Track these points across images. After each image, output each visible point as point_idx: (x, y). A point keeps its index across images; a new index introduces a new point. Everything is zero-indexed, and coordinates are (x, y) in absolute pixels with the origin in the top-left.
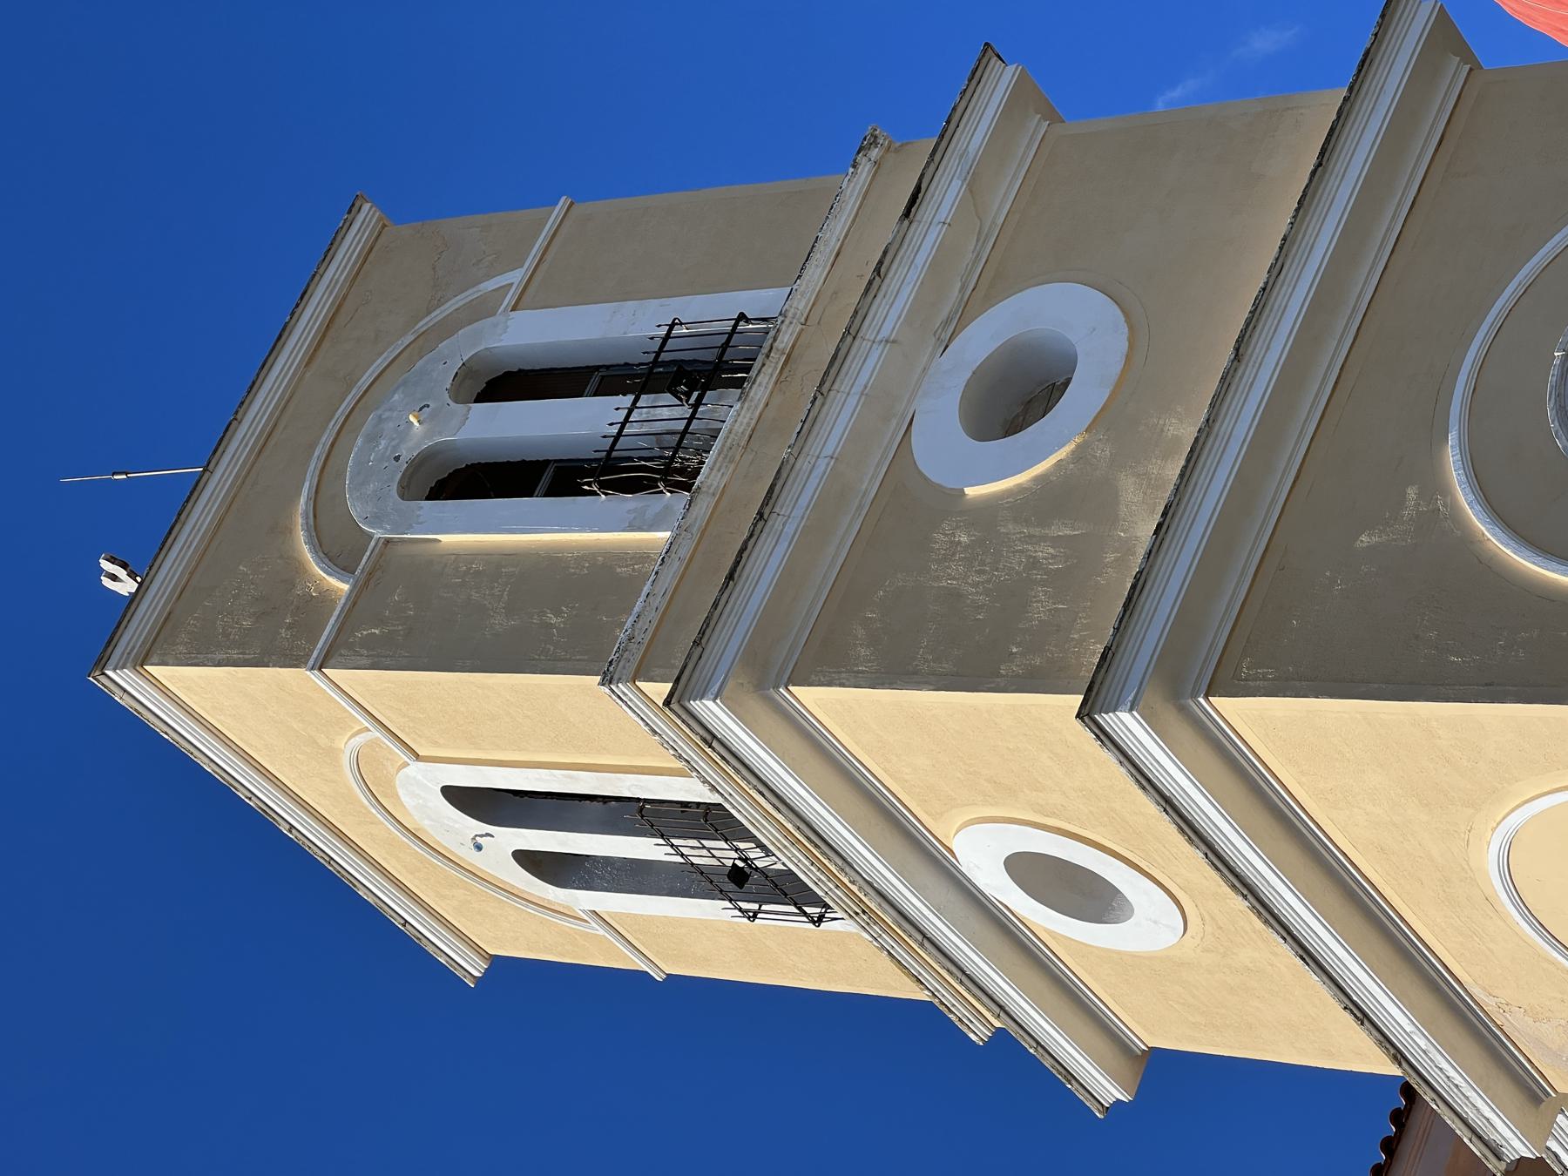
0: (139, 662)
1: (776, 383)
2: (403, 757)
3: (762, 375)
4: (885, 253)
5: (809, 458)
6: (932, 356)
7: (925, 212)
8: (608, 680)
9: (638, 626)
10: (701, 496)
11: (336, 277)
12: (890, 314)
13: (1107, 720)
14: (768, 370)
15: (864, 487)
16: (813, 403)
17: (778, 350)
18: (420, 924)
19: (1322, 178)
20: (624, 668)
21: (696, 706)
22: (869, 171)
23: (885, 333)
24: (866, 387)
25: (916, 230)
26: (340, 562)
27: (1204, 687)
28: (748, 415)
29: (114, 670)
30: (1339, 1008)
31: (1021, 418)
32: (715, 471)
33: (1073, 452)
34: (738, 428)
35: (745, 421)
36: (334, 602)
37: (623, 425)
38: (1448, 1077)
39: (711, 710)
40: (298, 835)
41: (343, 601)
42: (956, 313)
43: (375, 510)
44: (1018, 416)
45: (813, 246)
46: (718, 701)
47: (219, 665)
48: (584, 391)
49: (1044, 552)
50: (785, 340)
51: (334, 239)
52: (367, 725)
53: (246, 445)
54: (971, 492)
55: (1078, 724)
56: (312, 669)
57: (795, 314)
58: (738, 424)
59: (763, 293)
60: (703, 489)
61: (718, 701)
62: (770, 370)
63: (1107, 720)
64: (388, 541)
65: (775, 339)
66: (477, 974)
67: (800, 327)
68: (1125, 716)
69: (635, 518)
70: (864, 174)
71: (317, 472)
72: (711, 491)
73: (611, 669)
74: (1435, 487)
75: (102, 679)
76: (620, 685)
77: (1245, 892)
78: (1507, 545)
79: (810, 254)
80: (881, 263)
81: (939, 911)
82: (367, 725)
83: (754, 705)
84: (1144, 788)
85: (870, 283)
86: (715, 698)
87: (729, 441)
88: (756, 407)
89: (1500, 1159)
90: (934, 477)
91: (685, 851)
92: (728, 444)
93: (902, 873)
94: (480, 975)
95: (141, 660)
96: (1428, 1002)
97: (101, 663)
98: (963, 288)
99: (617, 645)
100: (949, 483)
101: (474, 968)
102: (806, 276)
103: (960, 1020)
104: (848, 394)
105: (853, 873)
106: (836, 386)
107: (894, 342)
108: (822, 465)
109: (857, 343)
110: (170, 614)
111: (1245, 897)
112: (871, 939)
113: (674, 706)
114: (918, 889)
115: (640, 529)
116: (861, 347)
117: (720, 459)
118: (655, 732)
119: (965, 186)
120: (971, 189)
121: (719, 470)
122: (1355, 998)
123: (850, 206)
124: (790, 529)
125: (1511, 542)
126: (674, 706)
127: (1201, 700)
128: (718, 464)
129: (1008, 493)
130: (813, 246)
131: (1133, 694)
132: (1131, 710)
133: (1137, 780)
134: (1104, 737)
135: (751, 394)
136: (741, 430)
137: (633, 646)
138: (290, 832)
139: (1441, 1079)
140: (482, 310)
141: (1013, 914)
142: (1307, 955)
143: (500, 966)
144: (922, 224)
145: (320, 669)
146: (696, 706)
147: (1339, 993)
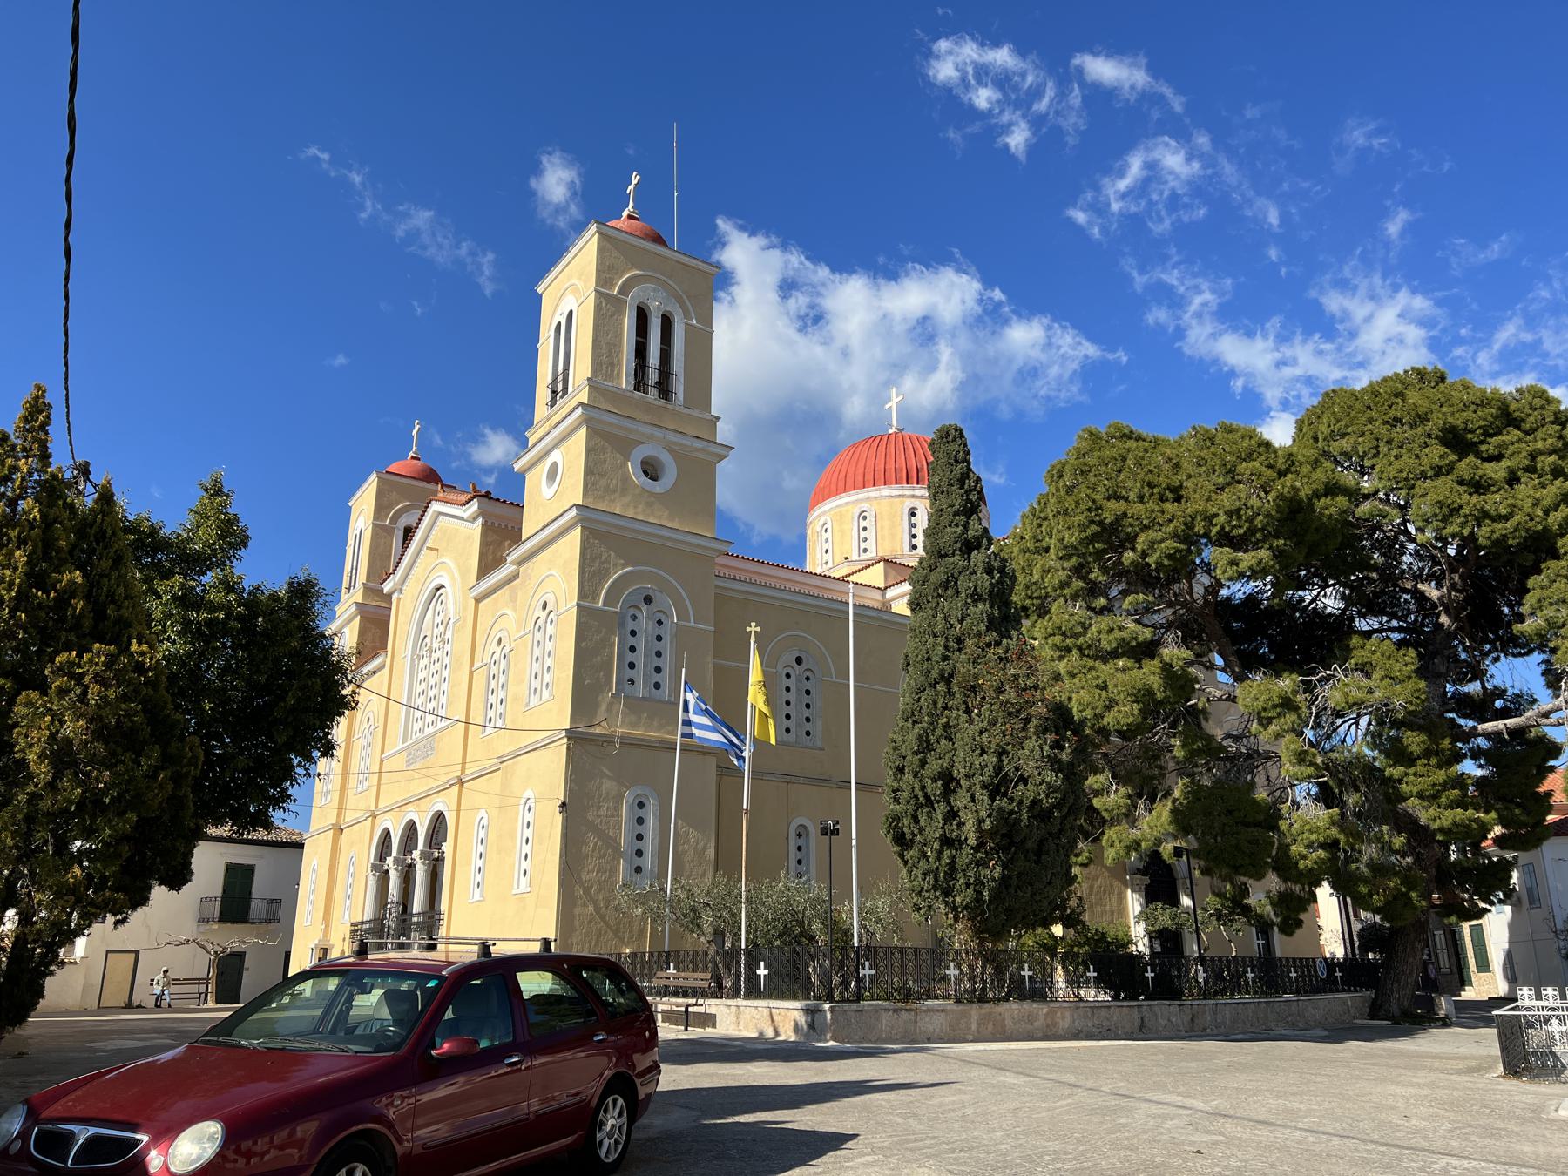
2: (580, 302)
8: (588, 379)
12: (671, 437)
18: (559, 268)
25: (692, 439)
26: (620, 292)
39: (579, 410)
48: (512, 886)
49: (614, 481)
50: (669, 406)
90: (634, 452)
95: (598, 232)
97: (597, 222)
100: (631, 457)
134: (571, 507)
140: (686, 315)
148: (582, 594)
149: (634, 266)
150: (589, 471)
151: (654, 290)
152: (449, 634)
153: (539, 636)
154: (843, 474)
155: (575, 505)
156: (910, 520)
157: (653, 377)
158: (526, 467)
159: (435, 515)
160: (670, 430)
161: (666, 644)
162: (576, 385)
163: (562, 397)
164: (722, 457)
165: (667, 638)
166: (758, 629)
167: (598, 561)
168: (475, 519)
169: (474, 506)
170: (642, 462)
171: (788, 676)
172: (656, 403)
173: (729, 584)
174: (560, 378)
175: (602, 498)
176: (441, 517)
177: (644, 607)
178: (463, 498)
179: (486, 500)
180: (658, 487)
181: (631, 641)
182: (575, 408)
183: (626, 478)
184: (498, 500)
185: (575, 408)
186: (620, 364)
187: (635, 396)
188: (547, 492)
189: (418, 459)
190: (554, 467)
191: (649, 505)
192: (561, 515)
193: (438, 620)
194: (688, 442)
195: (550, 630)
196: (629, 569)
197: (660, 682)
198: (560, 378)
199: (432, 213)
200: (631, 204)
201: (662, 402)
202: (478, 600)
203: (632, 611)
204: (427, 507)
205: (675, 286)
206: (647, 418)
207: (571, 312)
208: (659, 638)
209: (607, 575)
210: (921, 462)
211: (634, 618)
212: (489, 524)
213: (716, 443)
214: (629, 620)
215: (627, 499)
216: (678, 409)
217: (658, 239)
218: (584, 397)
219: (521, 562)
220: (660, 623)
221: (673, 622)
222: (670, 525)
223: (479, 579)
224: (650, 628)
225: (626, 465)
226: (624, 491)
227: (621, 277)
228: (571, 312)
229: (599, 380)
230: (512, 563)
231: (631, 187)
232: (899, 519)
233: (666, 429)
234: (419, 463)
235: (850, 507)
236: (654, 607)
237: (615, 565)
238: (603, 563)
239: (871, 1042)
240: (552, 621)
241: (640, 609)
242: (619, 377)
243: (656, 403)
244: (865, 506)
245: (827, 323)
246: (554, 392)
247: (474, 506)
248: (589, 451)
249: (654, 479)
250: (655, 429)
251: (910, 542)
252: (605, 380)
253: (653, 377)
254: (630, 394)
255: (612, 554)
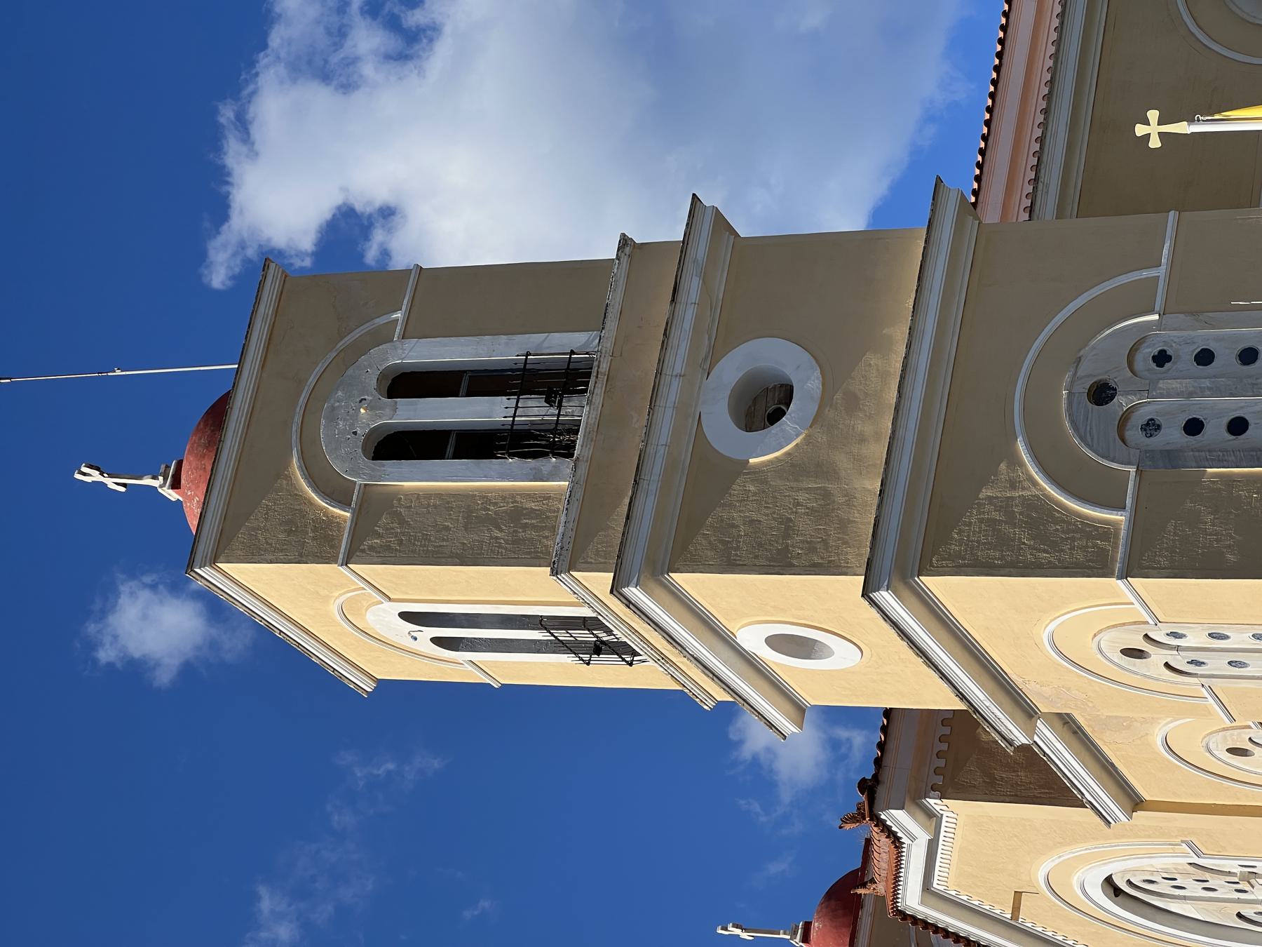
0: (212, 561)
1: (605, 393)
2: (378, 597)
4: (667, 323)
5: (652, 446)
6: (702, 378)
7: (682, 296)
8: (555, 572)
9: (564, 540)
10: (580, 463)
11: (267, 311)
12: (678, 360)
13: (876, 596)
14: (599, 385)
16: (649, 415)
17: (601, 373)
19: (920, 293)
20: (562, 564)
21: (625, 590)
22: (627, 261)
24: (675, 403)
25: (680, 307)
26: (344, 503)
27: (916, 573)
28: (595, 413)
29: (200, 568)
30: (953, 695)
31: (753, 408)
32: (584, 447)
33: (804, 439)
34: (591, 421)
35: (594, 416)
36: (339, 527)
37: (514, 416)
38: (999, 719)
39: (634, 592)
40: (285, 636)
41: (348, 524)
42: (709, 352)
43: (351, 466)
44: (750, 407)
45: (606, 309)
46: (638, 587)
47: (271, 562)
49: (802, 497)
50: (604, 367)
51: (259, 288)
52: (363, 586)
53: (240, 423)
55: (862, 600)
56: (342, 565)
57: (606, 351)
58: (590, 419)
60: (580, 459)
61: (638, 587)
62: (600, 386)
63: (876, 596)
64: (366, 485)
65: (599, 367)
66: (369, 690)
67: (610, 358)
68: (884, 593)
69: (536, 473)
71: (298, 440)
72: (585, 459)
73: (556, 566)
74: (1016, 462)
75: (192, 573)
76: (562, 575)
77: (921, 655)
78: (1061, 496)
79: (605, 314)
80: (666, 330)
81: (725, 663)
82: (363, 586)
83: (652, 585)
84: (886, 620)
85: (663, 342)
86: (637, 586)
87: (588, 430)
88: (598, 407)
89: (1011, 745)
91: (556, 635)
92: (588, 430)
93: (711, 649)
94: (371, 690)
95: (213, 561)
96: (991, 685)
97: (190, 566)
98: (709, 339)
99: (555, 553)
100: (736, 455)
101: (368, 686)
103: (701, 701)
104: (665, 407)
105: (685, 652)
106: (657, 403)
108: (662, 450)
110: (222, 530)
111: (921, 657)
112: (663, 670)
113: (615, 592)
114: (716, 654)
116: (665, 379)
117: (586, 440)
118: (575, 593)
119: (701, 281)
121: (586, 446)
122: (961, 690)
123: (621, 282)
124: (653, 487)
125: (1063, 494)
126: (615, 592)
127: (916, 578)
128: (585, 443)
129: (770, 462)
130: (606, 309)
131: (887, 582)
132: (887, 590)
133: (883, 618)
134: (873, 603)
135: (593, 401)
136: (592, 422)
137: (564, 552)
138: (280, 634)
139: (992, 717)
140: (382, 337)
141: (757, 656)
142: (943, 676)
143: (382, 684)
144: (682, 304)
145: (346, 565)
146: (625, 590)
147: (954, 690)
148: (1097, 566)
149: (281, 471)
150: (780, 563)
151: (332, 419)
152: (1233, 866)
153: (1216, 664)
155: (865, 594)
157: (535, 410)
158: (789, 707)
159: (933, 900)
160: (661, 361)
161: (1219, 339)
162: (573, 599)
163: (609, 632)
164: (721, 224)
165: (1204, 336)
166: (1153, 115)
167: (1005, 528)
168: (930, 814)
169: (898, 818)
170: (749, 428)
172: (598, 400)
173: (1053, 176)
174: (562, 635)
175: (844, 525)
176: (936, 885)
177: (1122, 402)
178: (882, 844)
179: (881, 792)
180: (808, 385)
181: (1215, 431)
182: (629, 603)
183: (793, 468)
184: (878, 762)
185: (629, 603)
186: (512, 495)
187: (587, 453)
188: (842, 656)
189: (807, 927)
190: (778, 643)
191: (853, 404)
192: (895, 625)
193: (1195, 890)
194: (688, 314)
195: (1195, 638)
196: (1021, 447)
197: (1226, 420)
198: (562, 635)
199: (263, 891)
200: (147, 481)
201: (597, 386)
202: (1135, 803)
203: (1134, 434)
204: (915, 920)
205: (319, 369)
206: (640, 421)
207: (405, 616)
208: (1205, 357)
209: (1041, 510)
211: (1151, 427)
212: (939, 780)
213: (685, 241)
214: (1158, 441)
215: (842, 461)
216: (608, 345)
217: (217, 415)
218: (600, 581)
219: (1027, 711)
220: (1162, 359)
221: (1158, 325)
222: (902, 350)
223: (1078, 803)
224: (1175, 384)
225: (758, 474)
226: (825, 471)
227: (310, 502)
228: (405, 616)
229: (554, 544)
230: (1031, 731)
231: (110, 483)
233: (659, 372)
234: (816, 925)
236: (1118, 376)
237: (1013, 485)
238: (1010, 515)
239: (1088, 679)
240: (1175, 635)
241: (1131, 410)
242: (545, 496)
243: (598, 400)
245: (281, 82)
246: (598, 648)
247: (898, 818)
248: (730, 564)
249: (786, 393)
250: (661, 402)
252: (553, 529)
253: (535, 410)
254: (583, 468)
255: (986, 492)
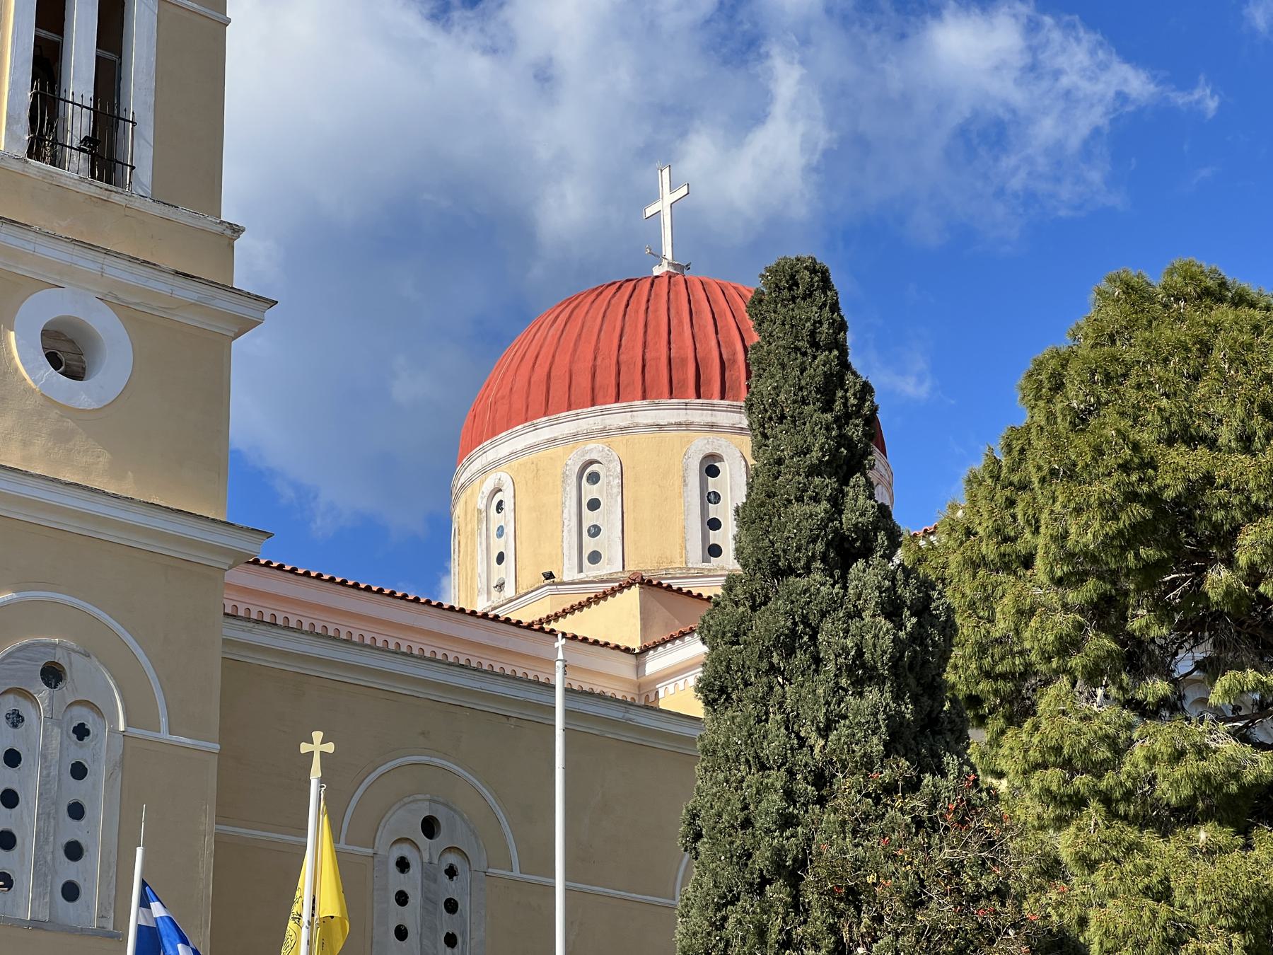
3: (95, 188)
4: (155, 265)
7: (180, 281)
14: (98, 190)
15: (20, 266)
23: (107, 269)
34: (63, 180)
50: (116, 198)
54: (12, 334)
59: (150, 173)
65: (116, 192)
67: (124, 205)
70: (215, 228)
85: (137, 259)
98: (137, 304)
102: (156, 205)
106: (76, 247)
107: (102, 276)
109: (103, 255)
115: (8, 123)
120: (192, 304)
129: (10, 352)
154: (541, 371)
156: (703, 485)
157: (77, 124)
166: (330, 748)
170: (45, 333)
171: (403, 865)
210: (731, 345)
220: (81, 732)
232: (678, 482)
235: (558, 450)
244: (594, 449)
251: (705, 537)
